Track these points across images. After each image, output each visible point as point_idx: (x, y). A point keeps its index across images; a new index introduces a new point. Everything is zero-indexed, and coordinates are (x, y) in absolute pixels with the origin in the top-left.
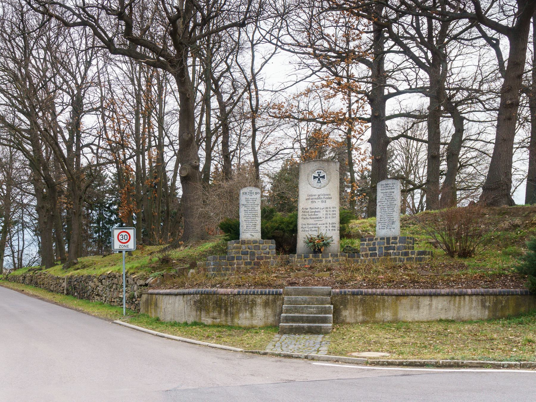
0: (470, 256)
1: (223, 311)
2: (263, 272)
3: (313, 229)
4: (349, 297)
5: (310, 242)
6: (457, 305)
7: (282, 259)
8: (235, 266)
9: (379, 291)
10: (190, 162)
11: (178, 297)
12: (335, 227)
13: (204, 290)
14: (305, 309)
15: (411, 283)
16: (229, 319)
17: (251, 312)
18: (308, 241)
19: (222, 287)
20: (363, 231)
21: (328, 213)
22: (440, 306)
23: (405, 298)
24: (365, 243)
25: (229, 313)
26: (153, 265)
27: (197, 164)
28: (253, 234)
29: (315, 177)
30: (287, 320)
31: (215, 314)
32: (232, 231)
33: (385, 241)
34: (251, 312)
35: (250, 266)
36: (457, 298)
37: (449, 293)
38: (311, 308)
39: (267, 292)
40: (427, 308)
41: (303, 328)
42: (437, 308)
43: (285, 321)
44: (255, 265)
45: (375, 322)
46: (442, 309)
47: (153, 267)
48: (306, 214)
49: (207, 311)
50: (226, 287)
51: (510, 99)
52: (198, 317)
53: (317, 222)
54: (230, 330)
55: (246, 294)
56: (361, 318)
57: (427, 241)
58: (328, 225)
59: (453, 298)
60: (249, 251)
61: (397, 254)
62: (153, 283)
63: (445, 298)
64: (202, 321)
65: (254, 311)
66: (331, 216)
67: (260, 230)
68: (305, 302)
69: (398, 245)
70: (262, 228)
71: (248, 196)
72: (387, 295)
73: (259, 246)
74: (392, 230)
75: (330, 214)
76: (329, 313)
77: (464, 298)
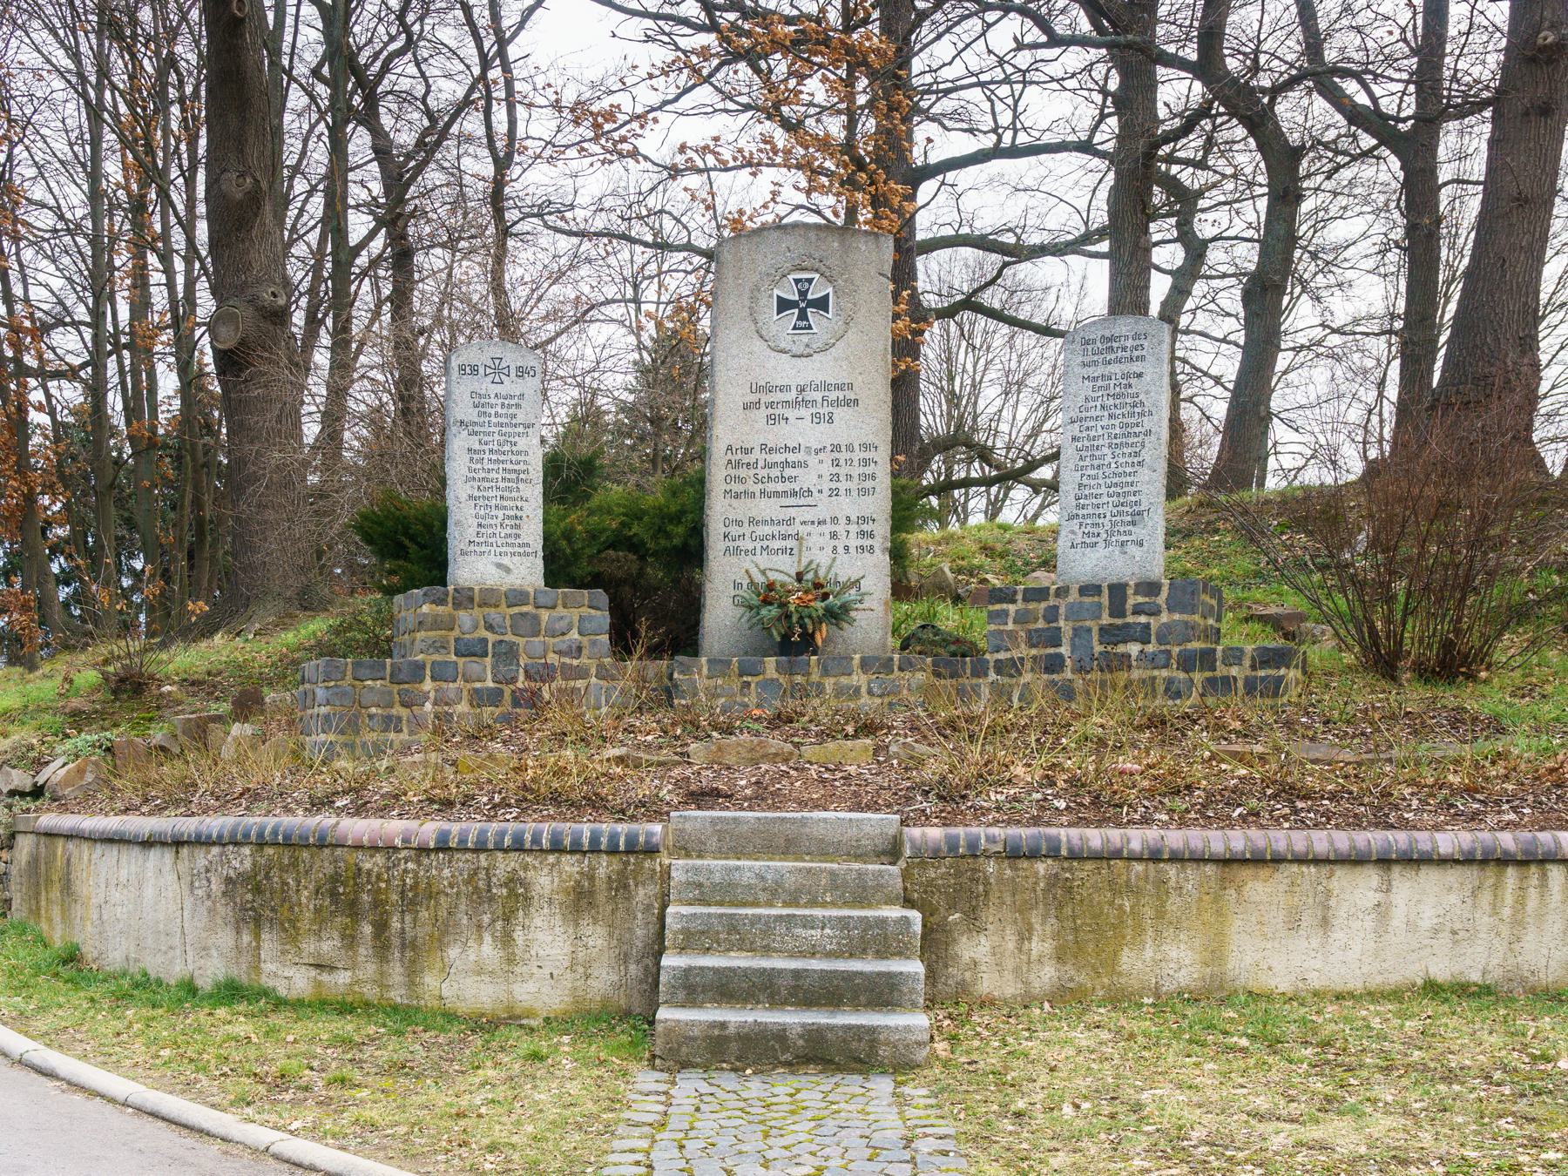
0: (1471, 677)
1: (367, 929)
2: (560, 737)
3: (776, 544)
4: (991, 867)
5: (767, 602)
6: (1506, 912)
7: (641, 680)
8: (428, 706)
9: (1137, 839)
10: (250, 291)
11: (154, 854)
12: (871, 535)
13: (271, 822)
14: (781, 929)
15: (1274, 796)
16: (396, 972)
17: (506, 940)
18: (755, 601)
19: (359, 810)
20: (959, 571)
21: (843, 471)
22: (1427, 920)
23: (1264, 872)
24: (1012, 608)
25: (396, 941)
26: (76, 703)
27: (281, 301)
28: (506, 561)
29: (784, 305)
30: (694, 989)
31: (329, 946)
32: (413, 548)
33: (1105, 599)
34: (506, 940)
35: (498, 711)
36: (1511, 872)
37: (1472, 852)
38: (808, 923)
39: (586, 842)
40: (1369, 923)
41: (781, 1035)
42: (1411, 926)
43: (681, 995)
44: (516, 703)
45: (1119, 999)
46: (1436, 931)
47: (76, 713)
48: (743, 472)
49: (290, 932)
50: (382, 811)
51: (1552, 27)
52: (245, 959)
53: (792, 512)
54: (400, 1033)
55: (480, 848)
56: (1046, 975)
57: (1243, 613)
58: (840, 529)
59: (1491, 872)
60: (492, 638)
61: (1162, 659)
62: (67, 782)
63: (1453, 875)
64: (266, 982)
65: (518, 935)
66: (853, 485)
67: (537, 544)
68: (774, 892)
69: (1164, 618)
70: (547, 538)
71: (485, 385)
72: (1176, 858)
73: (536, 619)
74: (1132, 549)
75: (849, 477)
76: (901, 953)
77: (1544, 876)
